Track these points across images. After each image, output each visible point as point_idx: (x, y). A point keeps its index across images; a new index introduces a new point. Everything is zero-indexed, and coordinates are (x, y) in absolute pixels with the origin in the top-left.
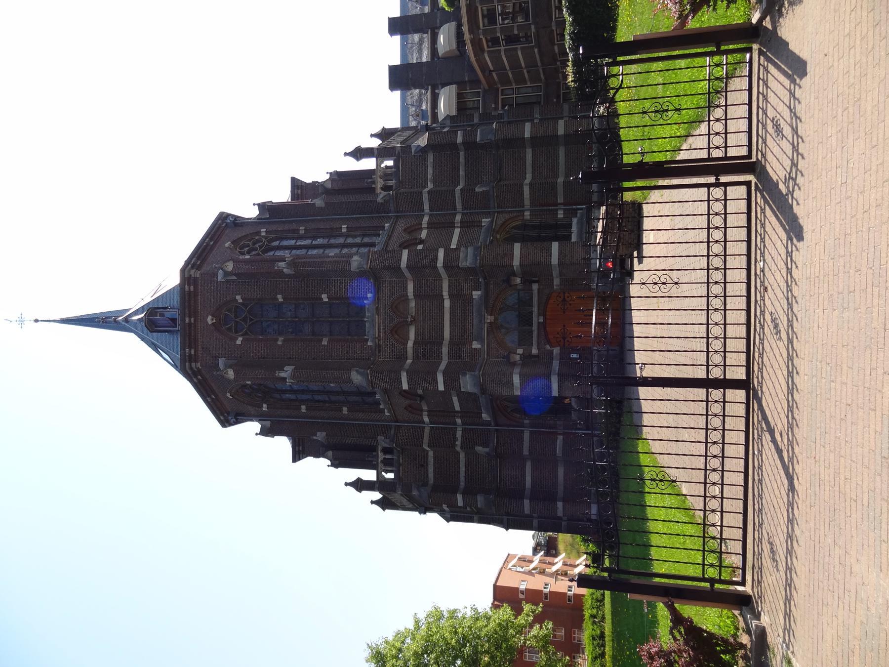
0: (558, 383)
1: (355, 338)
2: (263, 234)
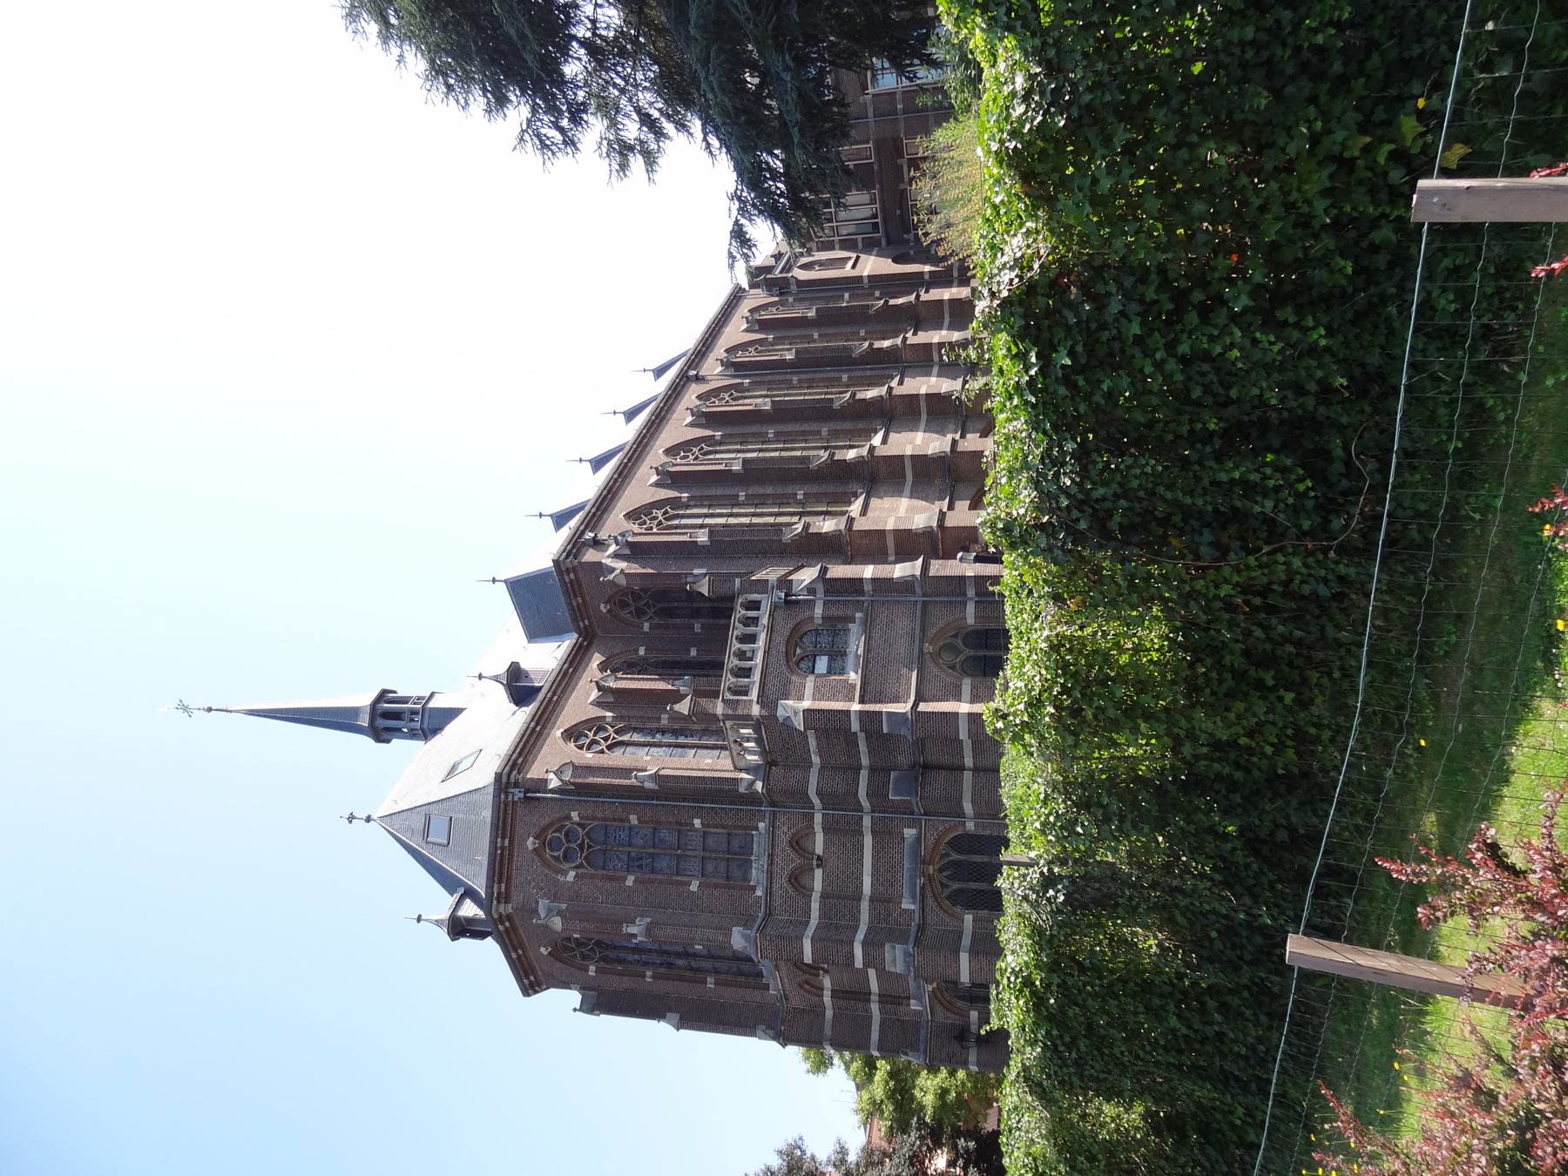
2: (592, 968)
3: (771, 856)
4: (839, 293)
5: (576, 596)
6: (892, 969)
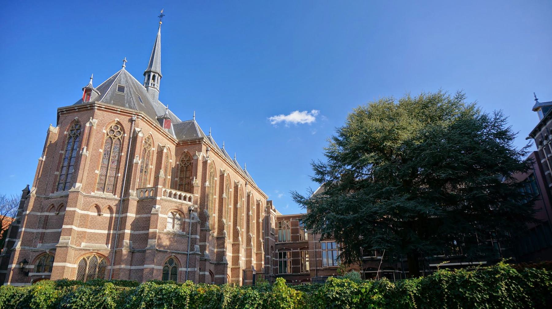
3: (105, 198)
4: (264, 229)
5: (191, 142)
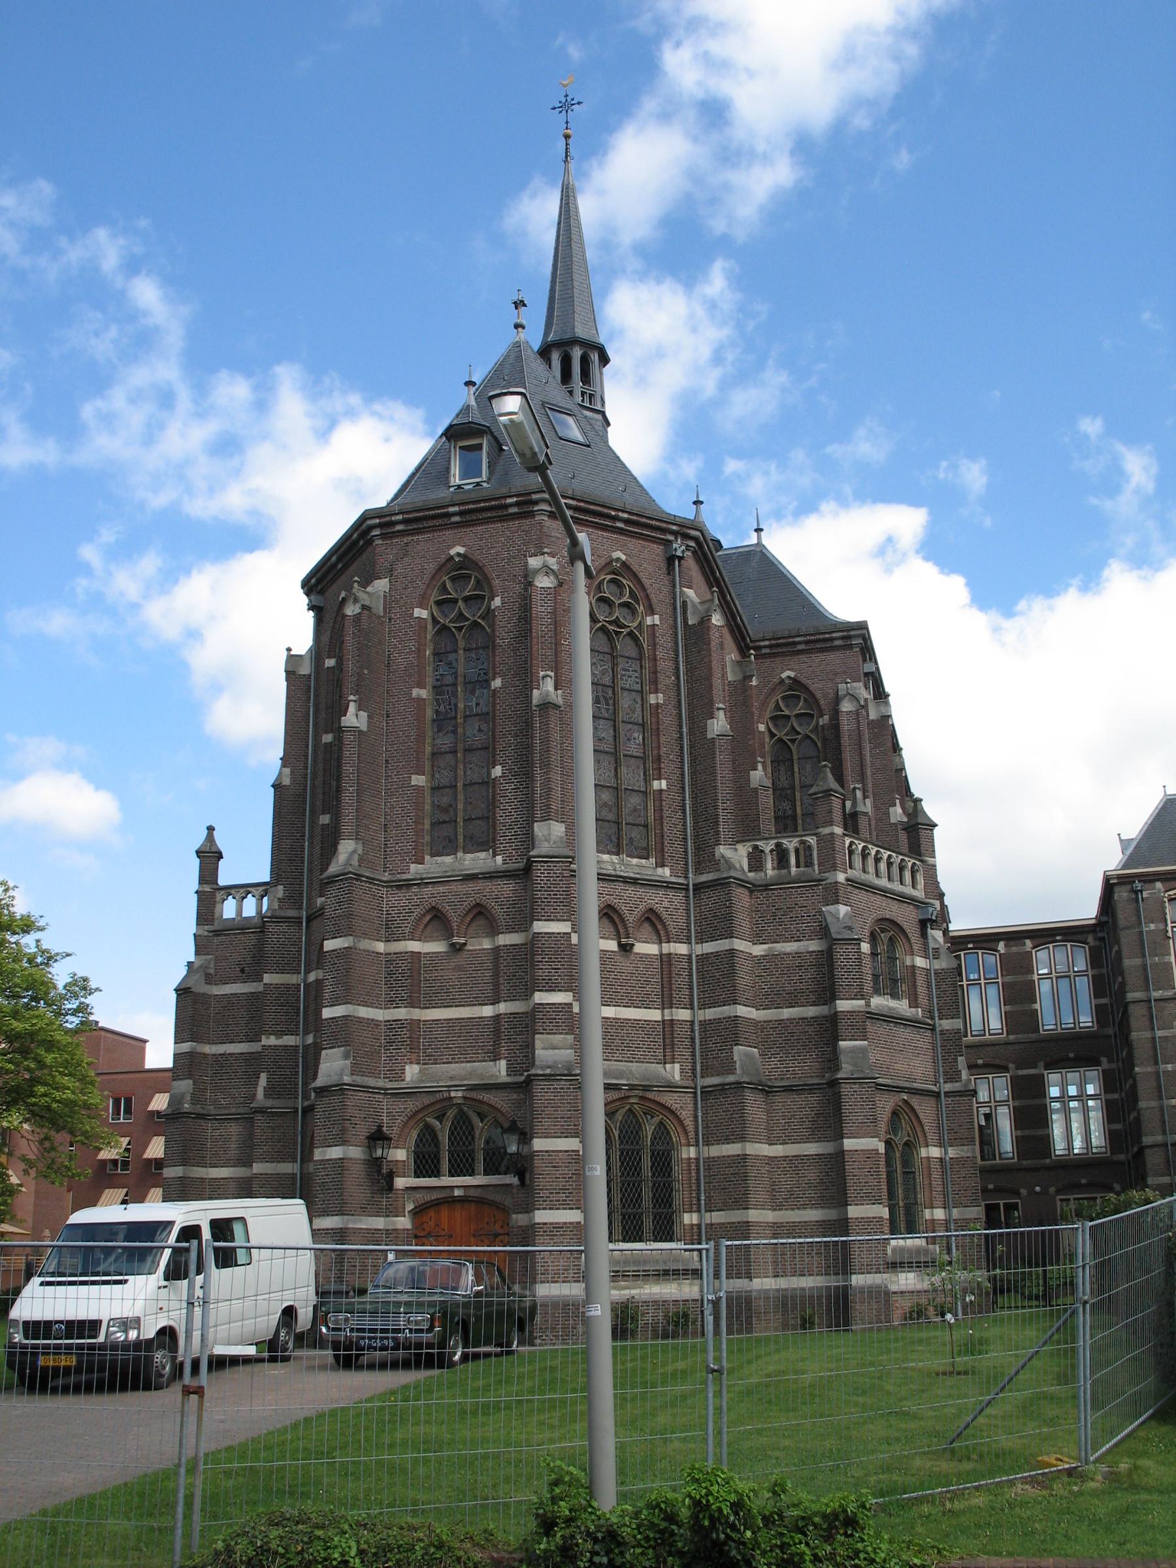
0: (332, 1229)
1: (427, 838)
2: (649, 621)
6: (538, 1044)
